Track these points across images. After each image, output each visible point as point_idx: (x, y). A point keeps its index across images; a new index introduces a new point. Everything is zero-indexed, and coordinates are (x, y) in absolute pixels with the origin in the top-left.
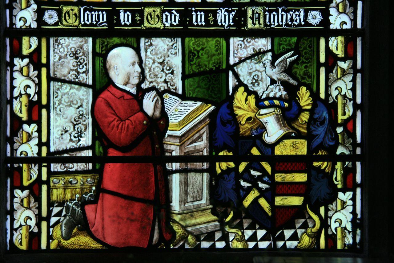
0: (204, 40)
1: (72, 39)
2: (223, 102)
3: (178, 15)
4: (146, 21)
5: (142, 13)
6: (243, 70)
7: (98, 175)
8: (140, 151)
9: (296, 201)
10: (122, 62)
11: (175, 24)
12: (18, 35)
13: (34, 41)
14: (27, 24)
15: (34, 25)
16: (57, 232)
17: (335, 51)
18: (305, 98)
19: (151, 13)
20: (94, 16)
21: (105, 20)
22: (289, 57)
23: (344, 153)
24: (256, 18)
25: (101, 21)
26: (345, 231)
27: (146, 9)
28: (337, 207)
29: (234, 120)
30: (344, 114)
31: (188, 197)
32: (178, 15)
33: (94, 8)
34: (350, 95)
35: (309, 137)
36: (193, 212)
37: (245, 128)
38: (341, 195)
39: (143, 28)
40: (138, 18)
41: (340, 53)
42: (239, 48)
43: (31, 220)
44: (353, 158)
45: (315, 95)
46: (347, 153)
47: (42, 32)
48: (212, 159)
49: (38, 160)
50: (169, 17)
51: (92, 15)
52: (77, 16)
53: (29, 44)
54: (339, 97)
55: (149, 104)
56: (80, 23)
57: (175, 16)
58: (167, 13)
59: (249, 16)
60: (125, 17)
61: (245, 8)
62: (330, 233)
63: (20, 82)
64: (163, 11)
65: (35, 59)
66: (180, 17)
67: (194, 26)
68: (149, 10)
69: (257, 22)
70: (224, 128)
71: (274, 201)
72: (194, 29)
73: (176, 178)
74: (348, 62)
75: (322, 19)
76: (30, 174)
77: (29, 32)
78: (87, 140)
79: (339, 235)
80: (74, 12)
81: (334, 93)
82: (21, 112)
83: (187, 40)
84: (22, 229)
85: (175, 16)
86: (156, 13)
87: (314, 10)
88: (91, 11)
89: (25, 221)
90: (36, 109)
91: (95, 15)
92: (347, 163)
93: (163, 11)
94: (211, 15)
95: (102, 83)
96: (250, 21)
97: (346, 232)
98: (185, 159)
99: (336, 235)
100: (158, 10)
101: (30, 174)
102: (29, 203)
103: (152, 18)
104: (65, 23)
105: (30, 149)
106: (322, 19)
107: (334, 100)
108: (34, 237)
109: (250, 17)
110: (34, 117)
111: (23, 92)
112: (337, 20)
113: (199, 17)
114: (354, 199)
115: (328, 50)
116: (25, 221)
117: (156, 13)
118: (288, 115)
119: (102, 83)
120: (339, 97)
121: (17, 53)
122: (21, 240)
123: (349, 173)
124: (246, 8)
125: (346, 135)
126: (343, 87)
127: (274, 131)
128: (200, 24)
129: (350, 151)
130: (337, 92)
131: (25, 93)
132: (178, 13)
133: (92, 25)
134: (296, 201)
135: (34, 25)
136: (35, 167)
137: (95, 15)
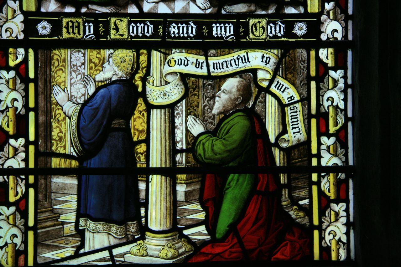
0: (68, 52)
3: (195, 27)
4: (251, 34)
5: (246, 25)
7: (286, 181)
11: (148, 35)
13: (21, 51)
14: (14, 35)
15: (21, 37)
17: (325, 60)
19: (256, 24)
20: (140, 29)
21: (232, 33)
23: (337, 164)
24: (71, 27)
25: (87, 33)
26: (340, 243)
27: (251, 20)
28: (330, 219)
30: (336, 124)
32: (195, 27)
34: (342, 105)
38: (334, 206)
39: (248, 40)
40: (102, 29)
41: (330, 62)
43: (17, 237)
46: (340, 164)
50: (273, 29)
51: (137, 27)
52: (264, 29)
54: (331, 109)
56: (267, 35)
57: (192, 27)
58: (271, 25)
59: (112, 27)
61: (108, 19)
62: (324, 245)
64: (268, 23)
66: (285, 28)
67: (171, 38)
68: (255, 21)
69: (76, 31)
71: (205, 216)
72: (156, 41)
74: (339, 72)
75: (37, 27)
77: (16, 43)
79: (333, 247)
80: (261, 25)
81: (326, 104)
82: (8, 126)
83: (321, 50)
84: (8, 247)
85: (280, 26)
86: (261, 25)
87: (300, 22)
88: (136, 23)
89: (12, 240)
91: (141, 27)
92: (340, 174)
93: (268, 23)
94: (160, 27)
96: (65, 30)
97: (340, 245)
99: (330, 247)
100: (263, 22)
102: (15, 220)
103: (256, 30)
104: (252, 36)
106: (37, 27)
107: (326, 111)
109: (65, 27)
111: (10, 105)
113: (228, 29)
114: (347, 210)
115: (318, 60)
116: (12, 240)
117: (261, 25)
120: (331, 108)
124: (248, 20)
125: (338, 145)
128: (182, 35)
129: (343, 162)
130: (331, 237)
131: (11, 242)
132: (195, 25)
133: (137, 36)
135: (21, 37)
136: (21, 183)
137: (141, 27)
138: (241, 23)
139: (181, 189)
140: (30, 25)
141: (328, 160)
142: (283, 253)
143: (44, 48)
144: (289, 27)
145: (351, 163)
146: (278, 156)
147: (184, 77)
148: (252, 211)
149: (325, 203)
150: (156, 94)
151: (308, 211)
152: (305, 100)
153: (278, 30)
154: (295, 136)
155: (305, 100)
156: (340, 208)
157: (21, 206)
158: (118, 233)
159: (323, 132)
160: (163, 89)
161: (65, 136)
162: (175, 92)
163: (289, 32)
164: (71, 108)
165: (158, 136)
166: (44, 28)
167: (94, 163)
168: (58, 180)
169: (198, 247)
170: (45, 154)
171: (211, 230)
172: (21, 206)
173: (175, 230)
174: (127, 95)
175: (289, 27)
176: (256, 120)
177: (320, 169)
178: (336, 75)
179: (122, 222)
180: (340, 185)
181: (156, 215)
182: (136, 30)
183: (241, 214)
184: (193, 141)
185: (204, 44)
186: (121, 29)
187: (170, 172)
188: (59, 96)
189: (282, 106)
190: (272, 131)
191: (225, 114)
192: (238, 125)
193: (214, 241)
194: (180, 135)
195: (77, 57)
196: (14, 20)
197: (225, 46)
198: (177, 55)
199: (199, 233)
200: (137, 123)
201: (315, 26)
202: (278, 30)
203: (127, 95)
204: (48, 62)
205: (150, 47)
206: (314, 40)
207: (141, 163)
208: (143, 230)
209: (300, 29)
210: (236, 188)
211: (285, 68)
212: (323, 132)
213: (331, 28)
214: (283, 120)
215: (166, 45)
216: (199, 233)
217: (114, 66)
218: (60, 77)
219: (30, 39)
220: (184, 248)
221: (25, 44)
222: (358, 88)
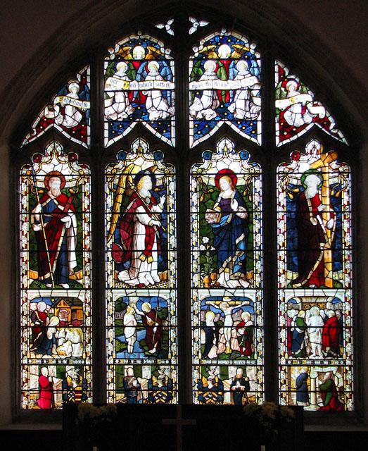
1: (255, 175)
2: (65, 379)
6: (68, 372)
8: (48, 389)
9: (80, 400)
10: (44, 371)
12: (24, 365)
16: (32, 405)
18: (81, 378)
22: (78, 370)
29: (67, 383)
31: (58, 400)
33: (311, 272)
35: (82, 386)
36: (41, 344)
37: (69, 384)
42: (68, 368)
44: (91, 391)
45: (83, 378)
47: (28, 364)
48: (63, 391)
49: (28, 391)
53: (26, 367)
55: (50, 379)
60: (45, 362)
63: (24, 374)
65: (320, 159)
70: (66, 386)
73: (55, 395)
76: (26, 393)
77: (26, 364)
78: (37, 386)
90: (27, 380)
95: (40, 375)
98: (57, 390)
101: (26, 393)
105: (26, 388)
108: (27, 407)
110: (27, 382)
112: (87, 363)
118: (78, 382)
119: (40, 375)
121: (281, 370)
122: (24, 407)
123: (175, 393)
126: (89, 376)
127: (75, 385)
134: (80, 400)
138: (329, 361)
139: (317, 396)
140: (287, 362)
141: (348, 390)
142: (339, 409)
143: (289, 366)
144: (340, 362)
145: (307, 428)
146: (338, 389)
147: (318, 372)
148: (332, 401)
149: (347, 399)
150: (312, 376)
151: (344, 400)
152: (343, 377)
153: (337, 363)
154: (341, 384)
155: (343, 377)
156: (350, 400)
157: (285, 398)
158: (321, 213)
159: (347, 384)
160: (313, 374)
161: (294, 385)
162: (316, 375)
163: (339, 363)
164: (295, 379)
165: (312, 385)
166: (289, 362)
167: (300, 390)
168: (292, 393)
169: (321, 407)
170: (290, 388)
171: (324, 404)
172: (285, 398)
173: (316, 404)
174: (306, 376)
175: (340, 362)
176: (333, 381)
177: (346, 392)
178: (349, 372)
179: (305, 402)
180: (350, 395)
181: (312, 401)
182: (308, 362)
183: (330, 401)
184: (320, 386)
185: (322, 365)
186: (305, 362)
187: (315, 392)
188: (292, 376)
189: (338, 379)
190: (336, 383)
191: (326, 380)
192: (330, 382)
193: (324, 406)
194: (317, 384)
195: (296, 368)
196: (205, 73)
197: (326, 366)
198: (316, 367)
199: (321, 405)
200: (308, 382)
201: (345, 362)
202: (337, 363)
203: (306, 376)
204: (290, 369)
205: (311, 366)
206: (345, 365)
207: (309, 390)
208: (310, 404)
209: (342, 362)
210: (329, 396)
211: (339, 370)
212: (347, 384)
213: (348, 362)
214: (339, 382)
215: (314, 365)
216: (321, 405)
217: (303, 370)
218: (292, 372)
219: (287, 365)
220: (318, 408)
221: (113, 365)
222: (354, 375)
